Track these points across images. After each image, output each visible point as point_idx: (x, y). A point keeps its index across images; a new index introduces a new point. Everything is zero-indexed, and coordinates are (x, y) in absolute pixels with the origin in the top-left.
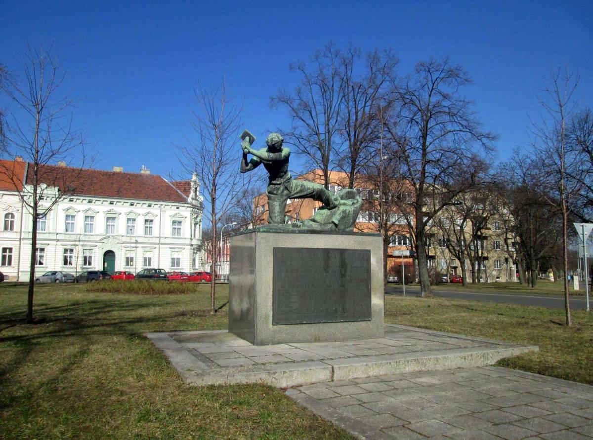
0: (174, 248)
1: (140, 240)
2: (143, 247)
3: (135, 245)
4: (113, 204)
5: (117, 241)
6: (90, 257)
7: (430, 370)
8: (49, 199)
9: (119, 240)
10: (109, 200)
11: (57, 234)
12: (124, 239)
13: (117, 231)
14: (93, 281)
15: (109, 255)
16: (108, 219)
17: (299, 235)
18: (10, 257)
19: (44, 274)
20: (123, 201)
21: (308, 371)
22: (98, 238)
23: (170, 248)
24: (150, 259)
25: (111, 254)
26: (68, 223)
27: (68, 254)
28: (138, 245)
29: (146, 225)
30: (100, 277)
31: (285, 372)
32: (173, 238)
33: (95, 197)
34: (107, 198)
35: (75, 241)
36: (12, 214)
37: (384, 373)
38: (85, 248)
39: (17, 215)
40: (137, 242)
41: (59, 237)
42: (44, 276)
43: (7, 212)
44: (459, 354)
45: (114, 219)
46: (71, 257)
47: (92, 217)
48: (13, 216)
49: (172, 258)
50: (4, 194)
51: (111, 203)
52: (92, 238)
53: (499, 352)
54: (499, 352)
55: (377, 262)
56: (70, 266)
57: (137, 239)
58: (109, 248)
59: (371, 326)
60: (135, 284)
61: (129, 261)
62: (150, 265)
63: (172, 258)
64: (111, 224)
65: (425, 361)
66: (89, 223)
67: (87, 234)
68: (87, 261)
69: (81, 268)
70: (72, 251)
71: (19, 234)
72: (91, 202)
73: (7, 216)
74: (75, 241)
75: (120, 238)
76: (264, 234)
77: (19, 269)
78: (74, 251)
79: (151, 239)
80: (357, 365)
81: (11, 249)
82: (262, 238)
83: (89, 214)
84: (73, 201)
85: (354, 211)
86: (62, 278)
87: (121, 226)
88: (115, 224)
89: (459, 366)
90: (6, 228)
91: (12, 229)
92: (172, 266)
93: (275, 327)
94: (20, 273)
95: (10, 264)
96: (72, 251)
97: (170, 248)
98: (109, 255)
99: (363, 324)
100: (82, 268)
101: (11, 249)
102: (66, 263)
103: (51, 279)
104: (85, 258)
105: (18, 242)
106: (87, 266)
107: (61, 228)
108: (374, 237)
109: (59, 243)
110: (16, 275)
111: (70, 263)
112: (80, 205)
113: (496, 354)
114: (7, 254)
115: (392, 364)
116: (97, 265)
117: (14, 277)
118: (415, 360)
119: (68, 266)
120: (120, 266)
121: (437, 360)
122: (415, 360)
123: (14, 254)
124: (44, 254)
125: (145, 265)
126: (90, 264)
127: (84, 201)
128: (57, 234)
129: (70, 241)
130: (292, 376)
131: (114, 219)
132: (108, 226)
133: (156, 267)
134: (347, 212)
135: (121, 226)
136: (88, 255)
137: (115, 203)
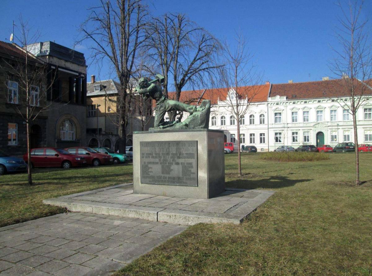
0: (366, 128)
1: (340, 124)
2: (303, 130)
3: (337, 127)
4: (320, 102)
5: (325, 126)
6: (308, 137)
7: (144, 219)
8: (281, 104)
9: (325, 124)
10: (317, 100)
11: (288, 124)
12: (329, 124)
13: (324, 119)
14: (306, 151)
15: (320, 135)
16: (318, 112)
17: (154, 134)
18: (264, 138)
19: (278, 147)
20: (313, 100)
21: (83, 206)
22: (312, 125)
23: (364, 128)
24: (348, 136)
25: (321, 134)
26: (332, 115)
27: (295, 135)
28: (339, 127)
29: (366, 113)
30: (309, 149)
31: (74, 205)
32: (365, 121)
33: (308, 99)
34: (316, 99)
35: (282, 128)
36: (263, 115)
37: (117, 215)
38: (305, 131)
39: (266, 115)
40: (338, 125)
41: (289, 125)
42: (278, 148)
43: (260, 114)
44: (166, 213)
45: (321, 111)
46: (280, 137)
47: (308, 112)
48: (264, 116)
49: (344, 135)
50: (258, 104)
51: (319, 102)
52: (308, 125)
53: (198, 218)
54: (198, 218)
55: (202, 149)
56: (297, 142)
57: (338, 123)
58: (322, 131)
59: (198, 190)
60: (297, 156)
61: (333, 138)
62: (348, 140)
63: (344, 135)
64: (320, 115)
65: (141, 213)
66: (306, 115)
67: (333, 121)
68: (306, 139)
69: (303, 143)
70: (280, 133)
71: (267, 125)
72: (306, 103)
73: (261, 116)
74: (282, 128)
75: (327, 123)
76: (137, 134)
77: (269, 145)
78: (282, 134)
79: (348, 123)
80: (103, 207)
81: (264, 134)
82: (135, 137)
83: (306, 110)
84: (306, 103)
85: (201, 115)
86: (286, 149)
87: (326, 116)
88: (323, 115)
89: (165, 221)
90: (261, 123)
91: (264, 123)
92: (365, 140)
93: (142, 185)
94: (270, 147)
95: (264, 142)
96: (280, 133)
97: (364, 128)
98: (320, 135)
99: (192, 189)
100: (303, 143)
101: (264, 134)
102: (294, 141)
103: (281, 150)
104: (305, 137)
105: (267, 130)
106: (307, 142)
107: (290, 120)
108: (200, 132)
109: (289, 129)
110: (267, 148)
111: (297, 141)
112: (299, 105)
113: (196, 219)
114: (263, 137)
115: (121, 210)
116: (313, 141)
117: (266, 149)
118: (135, 211)
119: (295, 142)
120: (327, 141)
121: (149, 214)
122: (135, 211)
123: (266, 137)
124: (298, 136)
125: (345, 140)
126: (308, 141)
127: (298, 103)
128: (288, 124)
129: (279, 128)
130: (76, 207)
131: (321, 111)
132: (318, 116)
133: (287, 145)
134: (196, 116)
135: (326, 116)
136: (307, 135)
137: (321, 101)
